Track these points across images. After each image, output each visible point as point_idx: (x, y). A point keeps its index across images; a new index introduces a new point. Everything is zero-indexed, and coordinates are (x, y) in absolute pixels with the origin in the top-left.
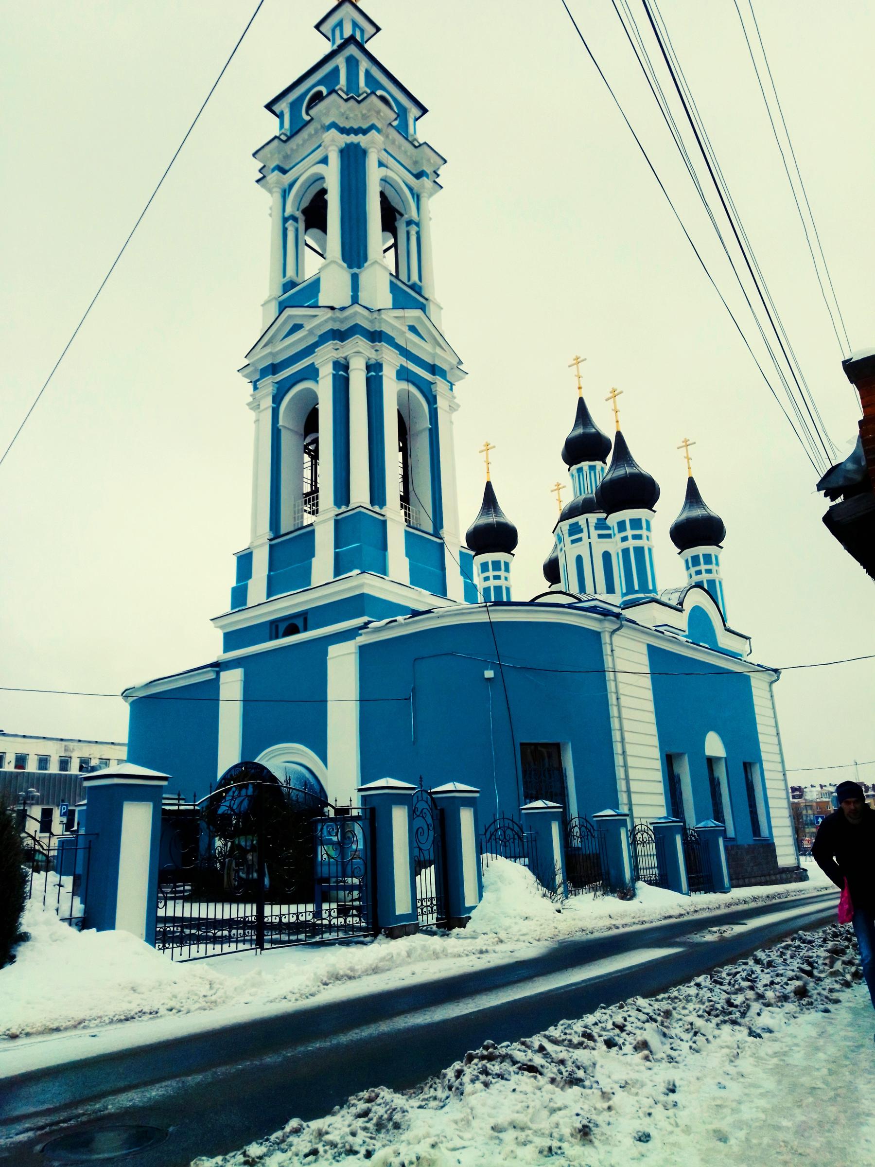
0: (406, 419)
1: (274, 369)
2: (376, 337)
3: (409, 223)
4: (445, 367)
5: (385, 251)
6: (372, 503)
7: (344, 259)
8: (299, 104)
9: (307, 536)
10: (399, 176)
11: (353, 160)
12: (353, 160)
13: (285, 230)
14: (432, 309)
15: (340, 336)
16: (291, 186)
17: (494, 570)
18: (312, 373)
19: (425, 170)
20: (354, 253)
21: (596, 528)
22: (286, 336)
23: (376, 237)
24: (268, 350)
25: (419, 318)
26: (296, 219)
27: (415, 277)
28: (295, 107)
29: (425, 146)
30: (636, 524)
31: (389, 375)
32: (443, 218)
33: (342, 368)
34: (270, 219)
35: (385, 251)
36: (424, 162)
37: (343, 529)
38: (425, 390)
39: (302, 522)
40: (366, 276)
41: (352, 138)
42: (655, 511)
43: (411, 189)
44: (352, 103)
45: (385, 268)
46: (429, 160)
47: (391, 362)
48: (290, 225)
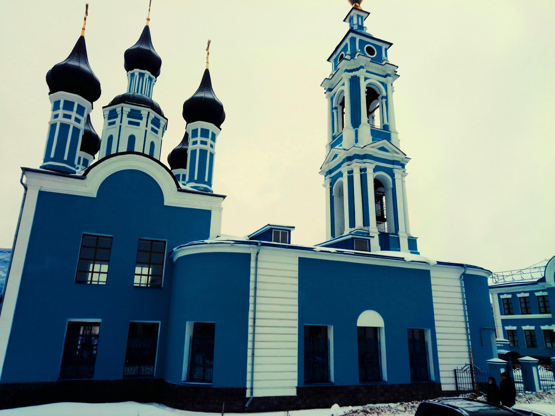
1: (330, 172)
6: (364, 226)
10: (374, 80)
15: (349, 159)
16: (334, 95)
17: (201, 136)
21: (129, 116)
26: (336, 108)
28: (335, 60)
30: (205, 133)
42: (221, 129)
43: (382, 83)
48: (334, 111)
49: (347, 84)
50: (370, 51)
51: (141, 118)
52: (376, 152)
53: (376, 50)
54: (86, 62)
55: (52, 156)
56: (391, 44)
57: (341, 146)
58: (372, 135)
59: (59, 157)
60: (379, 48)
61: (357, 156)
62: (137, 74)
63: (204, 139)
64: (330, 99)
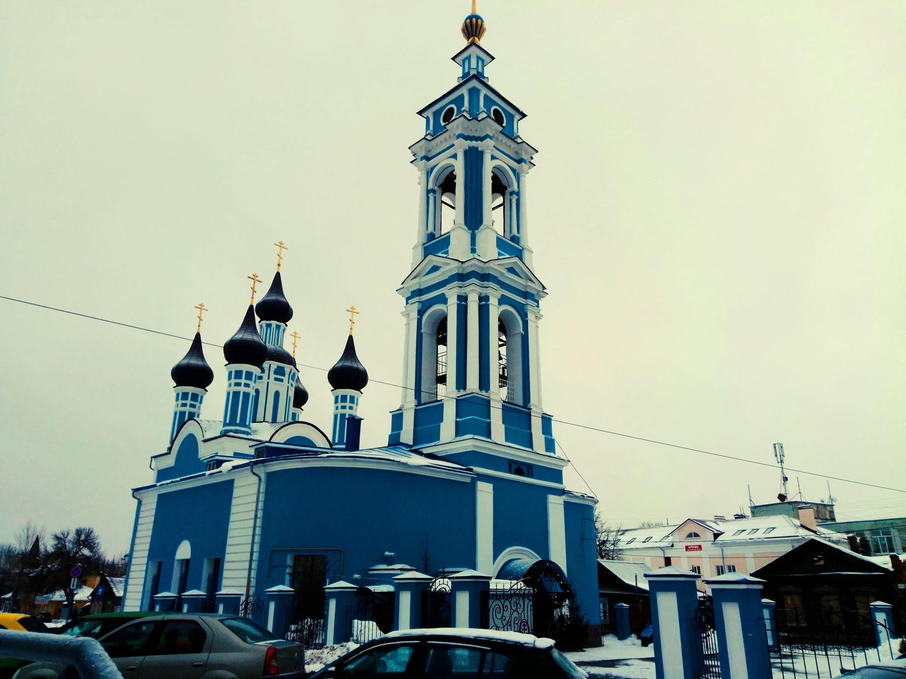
1: (419, 292)
2: (485, 277)
3: (512, 193)
4: (534, 293)
5: (494, 209)
6: (481, 388)
7: (466, 224)
8: (441, 114)
10: (504, 162)
11: (474, 159)
12: (474, 159)
13: (428, 198)
14: (526, 255)
15: (461, 277)
16: (433, 168)
17: (246, 378)
18: (443, 299)
19: (522, 156)
20: (474, 218)
21: (275, 373)
23: (490, 201)
24: (417, 280)
25: (515, 263)
26: (434, 191)
27: (515, 232)
28: (436, 114)
31: (493, 301)
32: (533, 185)
33: (463, 300)
35: (494, 209)
36: (523, 152)
37: (461, 405)
40: (481, 235)
41: (474, 143)
43: (514, 171)
46: (526, 151)
47: (494, 295)
48: (431, 195)
49: (461, 156)
50: (498, 118)
51: (284, 375)
52: (502, 274)
53: (506, 115)
54: (283, 296)
56: (524, 116)
57: (447, 253)
58: (498, 246)
59: (233, 422)
60: (511, 118)
61: (473, 274)
62: (274, 326)
63: (248, 382)
64: (425, 172)
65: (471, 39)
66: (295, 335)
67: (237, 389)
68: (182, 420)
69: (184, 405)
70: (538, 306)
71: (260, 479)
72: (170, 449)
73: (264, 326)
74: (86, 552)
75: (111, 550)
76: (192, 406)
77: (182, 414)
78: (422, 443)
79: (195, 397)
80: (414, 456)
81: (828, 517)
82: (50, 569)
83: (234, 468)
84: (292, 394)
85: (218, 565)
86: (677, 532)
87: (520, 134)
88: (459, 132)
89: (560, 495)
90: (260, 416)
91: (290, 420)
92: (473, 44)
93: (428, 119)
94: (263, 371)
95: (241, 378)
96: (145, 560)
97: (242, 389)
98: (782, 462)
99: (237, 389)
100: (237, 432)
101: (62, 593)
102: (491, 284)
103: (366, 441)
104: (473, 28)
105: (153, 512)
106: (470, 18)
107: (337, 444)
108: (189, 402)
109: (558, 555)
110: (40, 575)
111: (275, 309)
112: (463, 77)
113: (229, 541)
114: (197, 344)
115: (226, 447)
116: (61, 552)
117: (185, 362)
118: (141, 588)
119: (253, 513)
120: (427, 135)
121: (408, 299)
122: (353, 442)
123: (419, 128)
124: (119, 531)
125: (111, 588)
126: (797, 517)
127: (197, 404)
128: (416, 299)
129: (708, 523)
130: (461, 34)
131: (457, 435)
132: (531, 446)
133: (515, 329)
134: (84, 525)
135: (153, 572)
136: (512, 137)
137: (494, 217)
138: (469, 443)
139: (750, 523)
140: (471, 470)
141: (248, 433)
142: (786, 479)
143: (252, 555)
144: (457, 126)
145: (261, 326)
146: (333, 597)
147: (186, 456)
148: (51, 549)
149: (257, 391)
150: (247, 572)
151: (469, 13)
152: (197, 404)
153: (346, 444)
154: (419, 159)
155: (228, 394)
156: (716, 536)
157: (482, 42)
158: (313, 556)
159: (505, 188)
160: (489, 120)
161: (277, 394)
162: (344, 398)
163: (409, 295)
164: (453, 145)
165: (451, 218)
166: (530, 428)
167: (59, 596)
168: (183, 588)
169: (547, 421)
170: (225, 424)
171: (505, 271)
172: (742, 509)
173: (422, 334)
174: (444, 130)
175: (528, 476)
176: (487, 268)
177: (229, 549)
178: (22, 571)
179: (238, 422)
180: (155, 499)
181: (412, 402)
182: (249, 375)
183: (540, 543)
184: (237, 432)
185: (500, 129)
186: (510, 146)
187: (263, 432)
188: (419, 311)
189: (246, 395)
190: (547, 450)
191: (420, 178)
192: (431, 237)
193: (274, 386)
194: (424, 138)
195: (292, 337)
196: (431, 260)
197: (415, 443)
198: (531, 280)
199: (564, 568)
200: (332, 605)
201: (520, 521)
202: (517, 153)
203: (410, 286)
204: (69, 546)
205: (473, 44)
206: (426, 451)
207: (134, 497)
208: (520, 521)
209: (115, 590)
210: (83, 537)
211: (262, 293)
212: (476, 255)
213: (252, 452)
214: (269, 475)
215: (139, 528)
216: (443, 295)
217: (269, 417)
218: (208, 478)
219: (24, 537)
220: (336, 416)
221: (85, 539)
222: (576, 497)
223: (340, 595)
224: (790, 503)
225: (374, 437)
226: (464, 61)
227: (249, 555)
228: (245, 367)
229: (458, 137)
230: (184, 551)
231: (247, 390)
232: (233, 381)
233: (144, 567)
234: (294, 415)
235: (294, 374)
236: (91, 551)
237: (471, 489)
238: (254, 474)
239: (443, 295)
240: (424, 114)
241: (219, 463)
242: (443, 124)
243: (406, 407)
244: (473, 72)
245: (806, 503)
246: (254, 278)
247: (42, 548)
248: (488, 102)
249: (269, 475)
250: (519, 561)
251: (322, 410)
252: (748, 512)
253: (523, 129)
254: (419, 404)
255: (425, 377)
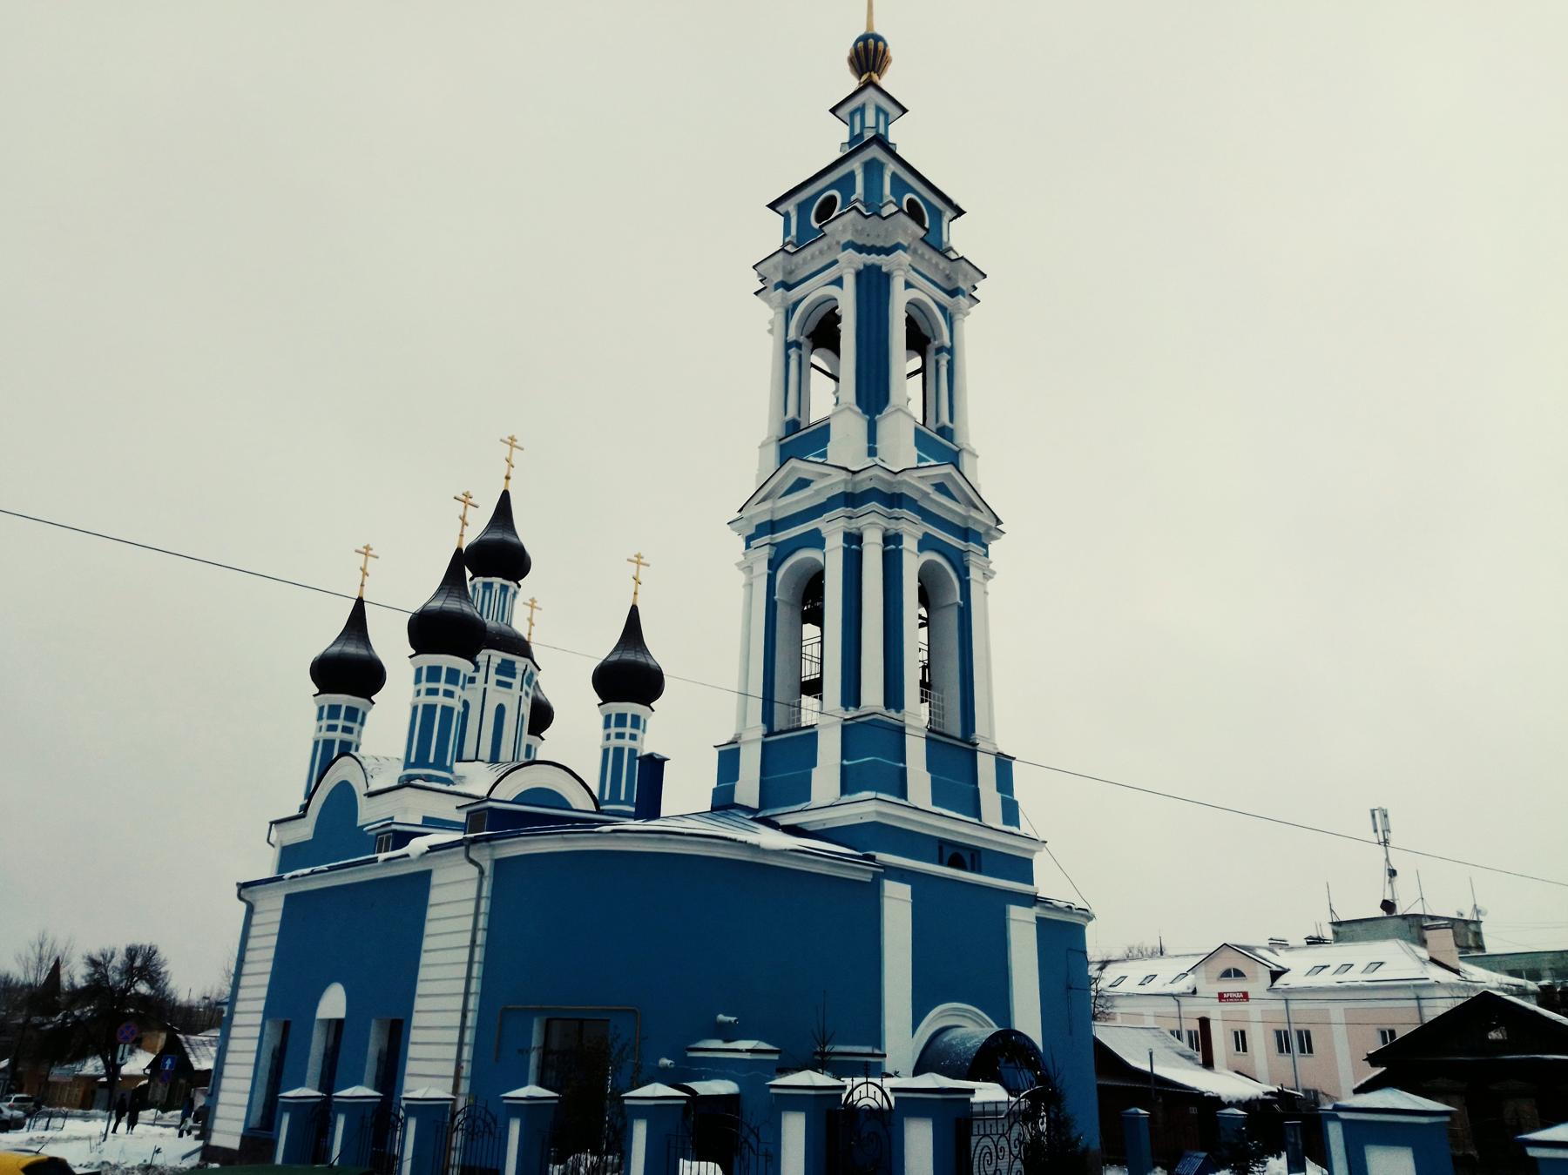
0: (928, 589)
1: (772, 527)
2: (895, 501)
3: (939, 350)
4: (981, 530)
5: (909, 375)
6: (887, 705)
7: (859, 402)
8: (810, 208)
9: (809, 739)
10: (927, 295)
11: (873, 287)
12: (873, 287)
13: (787, 357)
14: (966, 461)
15: (851, 499)
16: (796, 304)
18: (815, 540)
19: (958, 281)
20: (873, 394)
21: (498, 671)
22: (785, 495)
23: (903, 363)
24: (767, 505)
25: (949, 475)
26: (798, 345)
27: (945, 418)
28: (803, 208)
29: (963, 263)
31: (909, 545)
32: (978, 336)
33: (854, 541)
34: (770, 339)
35: (909, 375)
36: (961, 277)
37: (851, 735)
38: (957, 563)
39: (799, 720)
41: (873, 259)
43: (943, 309)
44: (875, 219)
45: (910, 416)
47: (912, 532)
48: (793, 352)
49: (850, 281)
50: (914, 212)
51: (513, 676)
52: (926, 495)
53: (929, 209)
55: (412, 760)
57: (824, 455)
58: (917, 444)
59: (422, 761)
60: (937, 215)
62: (496, 586)
63: (450, 687)
64: (782, 311)
65: (865, 77)
66: (532, 604)
67: (431, 700)
68: (327, 756)
69: (332, 728)
70: (986, 555)
71: (482, 872)
72: (305, 808)
73: (479, 586)
74: (143, 988)
75: (190, 981)
76: (347, 730)
77: (329, 744)
78: (776, 806)
79: (352, 714)
80: (763, 829)
81: (1471, 943)
82: (78, 1018)
83: (433, 848)
84: (526, 710)
85: (397, 1032)
86: (1202, 968)
87: (953, 243)
88: (848, 237)
89: (1030, 906)
90: (469, 751)
91: (523, 759)
92: (870, 83)
93: (787, 216)
94: (477, 669)
95: (438, 680)
96: (259, 1019)
97: (440, 700)
98: (1386, 842)
99: (431, 700)
100: (428, 778)
101: (100, 1062)
102: (905, 513)
103: (671, 803)
104: (869, 57)
105: (276, 928)
106: (864, 38)
107: (608, 803)
108: (340, 723)
109: (1028, 1019)
110: (60, 1030)
111: (498, 556)
112: (850, 143)
113: (421, 988)
114: (357, 623)
115: (410, 808)
116: (98, 988)
117: (337, 649)
118: (249, 1071)
119: (468, 936)
120: (785, 244)
121: (749, 539)
122: (649, 804)
123: (770, 233)
124: (206, 947)
125: (186, 1056)
126: (1423, 943)
127: (356, 726)
128: (766, 539)
129: (1259, 952)
130: (847, 67)
131: (844, 791)
132: (978, 815)
133: (949, 600)
134: (143, 940)
135: (273, 1041)
136: (943, 251)
137: (907, 390)
138: (866, 808)
139: (1335, 954)
140: (872, 858)
141: (448, 782)
142: (1393, 873)
143: (464, 1016)
144: (843, 227)
145: (474, 587)
146: (640, 1117)
147: (335, 825)
148: (80, 982)
149: (466, 704)
150: (455, 1049)
151: (862, 31)
152: (356, 726)
153: (637, 805)
154: (771, 287)
155: (415, 709)
156: (1275, 975)
157: (885, 82)
158: (581, 1021)
159: (927, 341)
160: (902, 217)
161: (501, 710)
162: (621, 719)
163: (752, 531)
164: (836, 262)
165: (826, 397)
166: (975, 780)
167: (93, 1066)
168: (328, 1082)
169: (1004, 764)
170: (408, 765)
171: (930, 490)
172: (1319, 926)
173: (775, 603)
174: (820, 235)
175: (973, 870)
176: (900, 483)
177: (419, 1004)
178: (27, 1021)
179: (431, 760)
180: (280, 903)
181: (756, 730)
182: (453, 675)
183: (997, 1000)
184: (428, 778)
185: (922, 233)
186: (937, 265)
187: (476, 779)
188: (770, 561)
189: (447, 711)
190: (1006, 822)
191: (771, 322)
192: (793, 426)
193: (496, 696)
194: (782, 249)
195: (531, 608)
196: (793, 469)
197: (764, 803)
198: (976, 508)
199: (1041, 1047)
200: (640, 1131)
201: (961, 955)
202: (948, 277)
203: (756, 515)
204: (114, 977)
205: (870, 83)
206: (784, 821)
207: (240, 897)
208: (961, 955)
209: (192, 1059)
210: (138, 963)
211: (477, 526)
212: (877, 460)
213: (461, 817)
214: (499, 864)
215: (249, 956)
216: (817, 531)
217: (486, 752)
218: (385, 864)
219: (33, 959)
220: (606, 752)
221: (143, 964)
222: (1057, 909)
223: (654, 1112)
224: (1404, 917)
225: (686, 793)
226: (852, 114)
227: (459, 1015)
228: (446, 661)
229: (845, 247)
230: (333, 1003)
231: (448, 702)
232: (424, 685)
233: (256, 1032)
234: (529, 747)
235: (532, 674)
236: (152, 987)
237: (870, 896)
238: (472, 861)
239: (817, 531)
240: (781, 208)
241: (402, 838)
242: (816, 226)
243: (746, 737)
244: (869, 135)
245: (1433, 918)
246: (466, 500)
247: (65, 980)
248: (899, 186)
249: (499, 864)
250: (959, 1031)
251: (579, 738)
252: (1328, 933)
253: (958, 236)
254: (770, 732)
255: (781, 684)
